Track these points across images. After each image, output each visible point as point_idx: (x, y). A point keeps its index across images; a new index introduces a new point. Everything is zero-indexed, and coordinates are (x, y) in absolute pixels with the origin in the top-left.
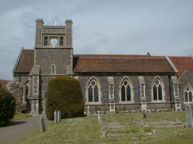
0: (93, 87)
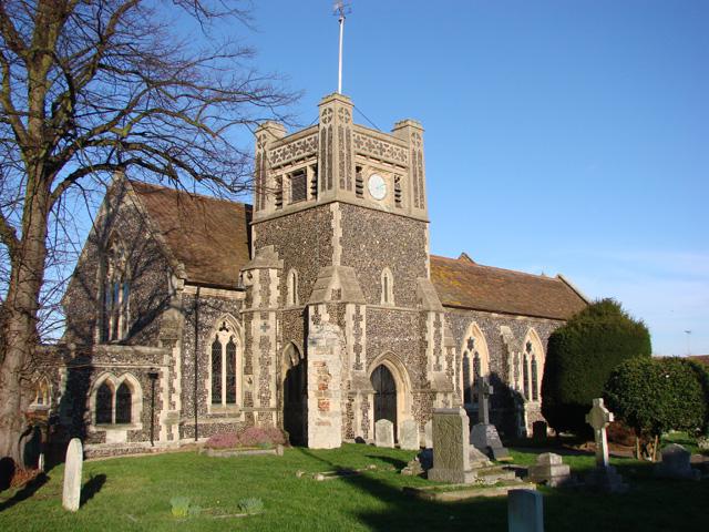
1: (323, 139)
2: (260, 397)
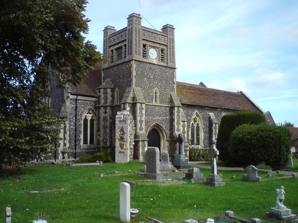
0: (195, 125)
1: (129, 33)
2: (103, 141)
